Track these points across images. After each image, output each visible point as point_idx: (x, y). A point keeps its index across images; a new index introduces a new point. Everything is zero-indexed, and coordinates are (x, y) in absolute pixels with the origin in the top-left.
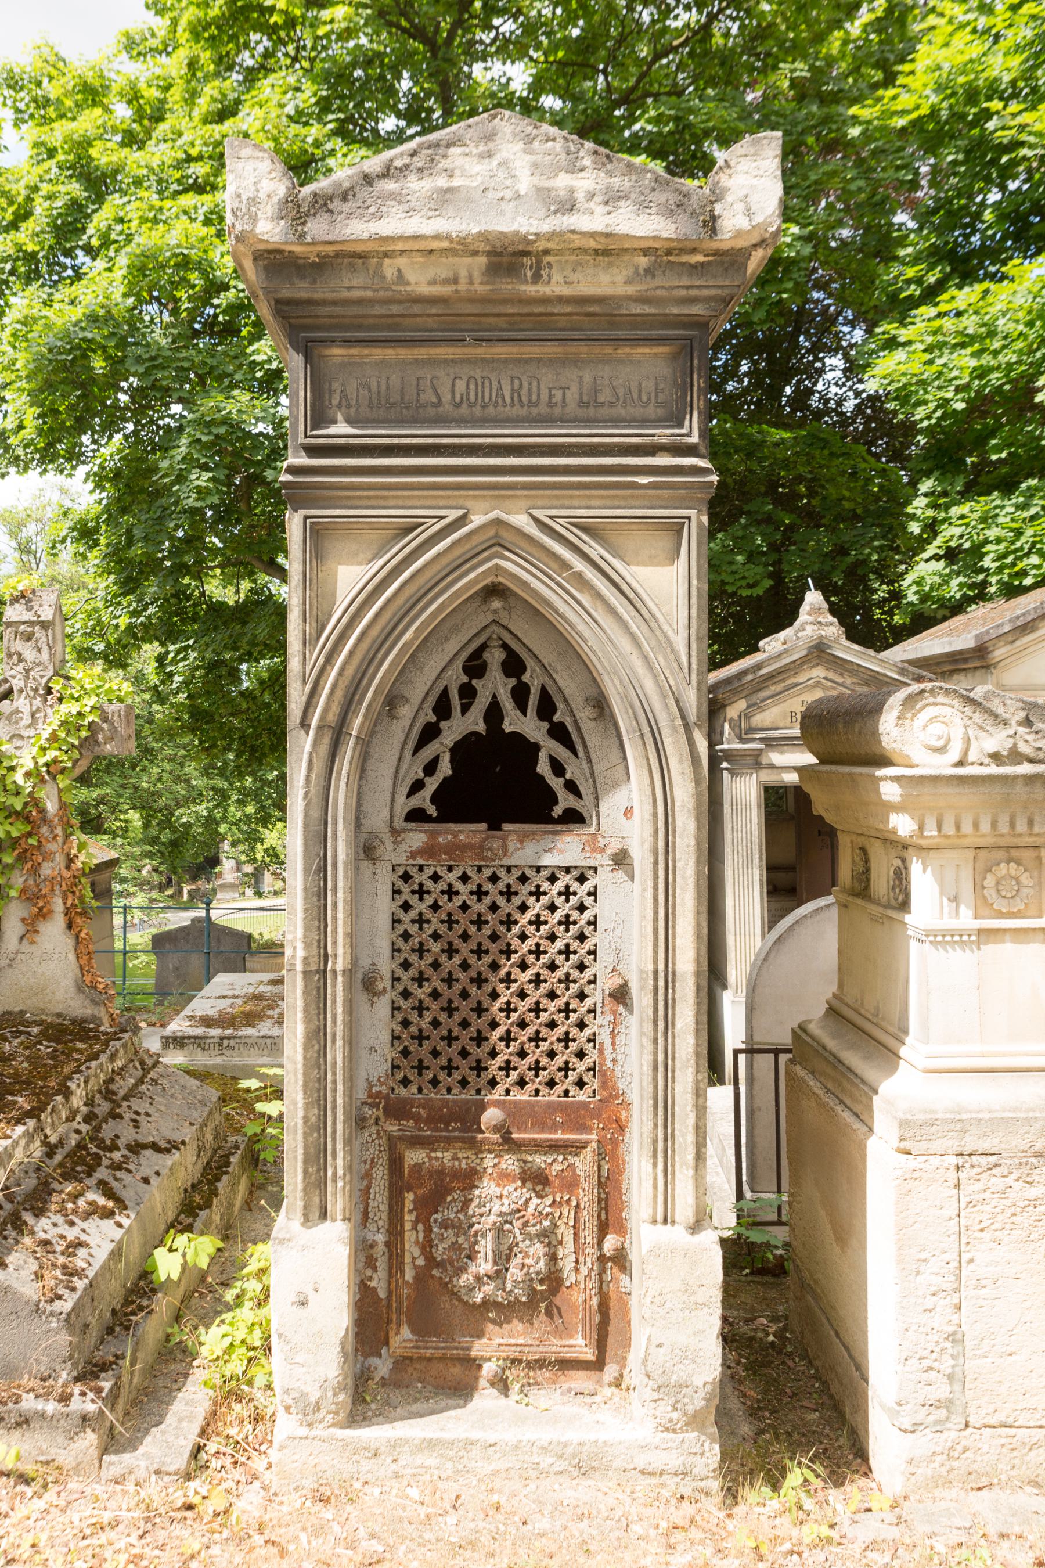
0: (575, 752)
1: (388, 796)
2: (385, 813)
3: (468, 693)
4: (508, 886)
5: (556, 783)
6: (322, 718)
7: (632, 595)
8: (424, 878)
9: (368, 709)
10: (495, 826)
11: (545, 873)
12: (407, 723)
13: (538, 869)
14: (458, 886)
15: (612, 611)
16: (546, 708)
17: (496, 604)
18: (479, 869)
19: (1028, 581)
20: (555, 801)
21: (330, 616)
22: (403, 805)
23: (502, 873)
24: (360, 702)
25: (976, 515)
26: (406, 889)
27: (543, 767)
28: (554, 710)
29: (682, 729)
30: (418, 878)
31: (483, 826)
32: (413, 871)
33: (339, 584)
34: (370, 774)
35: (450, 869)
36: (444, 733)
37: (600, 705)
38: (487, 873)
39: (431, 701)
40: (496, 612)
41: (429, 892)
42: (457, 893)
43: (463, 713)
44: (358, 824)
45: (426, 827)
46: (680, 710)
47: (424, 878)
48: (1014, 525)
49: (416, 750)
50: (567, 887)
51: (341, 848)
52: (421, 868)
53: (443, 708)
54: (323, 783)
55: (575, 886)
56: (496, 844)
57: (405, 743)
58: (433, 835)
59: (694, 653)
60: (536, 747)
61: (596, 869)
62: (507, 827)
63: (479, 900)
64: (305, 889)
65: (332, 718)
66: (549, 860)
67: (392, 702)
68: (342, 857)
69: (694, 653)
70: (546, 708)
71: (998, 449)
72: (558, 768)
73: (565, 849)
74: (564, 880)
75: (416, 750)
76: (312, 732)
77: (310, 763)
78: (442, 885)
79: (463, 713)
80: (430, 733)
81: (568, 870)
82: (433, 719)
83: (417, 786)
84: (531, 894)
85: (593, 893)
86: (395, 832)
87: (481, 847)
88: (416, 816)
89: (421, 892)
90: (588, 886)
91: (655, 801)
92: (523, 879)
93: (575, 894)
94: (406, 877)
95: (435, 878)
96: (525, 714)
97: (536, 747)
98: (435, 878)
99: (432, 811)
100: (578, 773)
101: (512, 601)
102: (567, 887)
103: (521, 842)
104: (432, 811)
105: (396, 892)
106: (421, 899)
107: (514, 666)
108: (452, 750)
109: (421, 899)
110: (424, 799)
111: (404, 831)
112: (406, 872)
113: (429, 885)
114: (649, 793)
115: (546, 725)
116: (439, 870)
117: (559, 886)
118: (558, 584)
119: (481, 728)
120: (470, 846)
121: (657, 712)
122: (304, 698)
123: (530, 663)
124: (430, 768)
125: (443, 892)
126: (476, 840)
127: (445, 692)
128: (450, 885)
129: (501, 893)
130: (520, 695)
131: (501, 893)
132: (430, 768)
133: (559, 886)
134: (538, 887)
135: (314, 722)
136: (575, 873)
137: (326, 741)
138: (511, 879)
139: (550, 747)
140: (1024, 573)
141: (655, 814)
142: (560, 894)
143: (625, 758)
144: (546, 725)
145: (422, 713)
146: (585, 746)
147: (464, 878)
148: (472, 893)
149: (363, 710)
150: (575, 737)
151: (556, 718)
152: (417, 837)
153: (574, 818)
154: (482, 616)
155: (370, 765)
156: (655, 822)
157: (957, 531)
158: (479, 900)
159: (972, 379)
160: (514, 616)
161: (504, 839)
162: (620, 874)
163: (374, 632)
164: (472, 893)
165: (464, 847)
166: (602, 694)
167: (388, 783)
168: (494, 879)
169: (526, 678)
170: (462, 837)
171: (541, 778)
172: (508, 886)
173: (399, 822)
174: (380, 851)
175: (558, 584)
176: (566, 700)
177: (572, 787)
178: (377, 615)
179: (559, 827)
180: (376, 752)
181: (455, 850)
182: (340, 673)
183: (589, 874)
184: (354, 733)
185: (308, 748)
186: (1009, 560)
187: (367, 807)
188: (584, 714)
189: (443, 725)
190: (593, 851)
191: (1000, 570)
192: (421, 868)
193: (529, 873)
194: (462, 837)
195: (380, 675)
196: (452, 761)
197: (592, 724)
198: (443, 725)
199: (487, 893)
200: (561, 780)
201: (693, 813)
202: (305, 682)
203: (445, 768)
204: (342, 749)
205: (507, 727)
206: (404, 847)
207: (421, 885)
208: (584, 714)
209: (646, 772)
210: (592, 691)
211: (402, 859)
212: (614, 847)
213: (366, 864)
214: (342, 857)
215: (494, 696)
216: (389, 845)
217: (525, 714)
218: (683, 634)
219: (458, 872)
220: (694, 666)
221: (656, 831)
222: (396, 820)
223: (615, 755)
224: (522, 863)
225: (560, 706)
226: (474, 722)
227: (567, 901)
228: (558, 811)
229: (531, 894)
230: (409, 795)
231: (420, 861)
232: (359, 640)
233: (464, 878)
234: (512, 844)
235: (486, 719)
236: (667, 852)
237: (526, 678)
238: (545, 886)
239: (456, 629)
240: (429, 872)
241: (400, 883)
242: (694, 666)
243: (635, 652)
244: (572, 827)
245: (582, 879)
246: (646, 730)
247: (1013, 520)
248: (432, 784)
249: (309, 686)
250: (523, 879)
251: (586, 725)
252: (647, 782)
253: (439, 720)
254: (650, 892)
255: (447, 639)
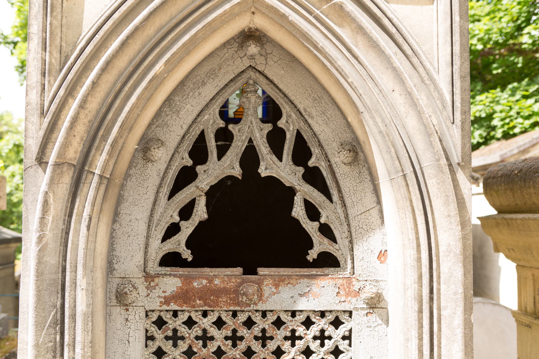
0: (329, 197)
1: (142, 240)
2: (139, 258)
3: (224, 137)
4: (264, 331)
5: (311, 228)
6: (60, 155)
7: (393, 30)
8: (178, 323)
9: (113, 146)
10: (250, 270)
11: (301, 318)
12: (163, 167)
13: (294, 314)
14: (213, 331)
15: (374, 45)
16: (301, 154)
17: (253, 49)
18: (235, 314)
19: (517, 130)
20: (311, 246)
21: (75, 47)
22: (158, 249)
23: (257, 318)
24: (105, 138)
25: (489, 100)
26: (159, 335)
27: (298, 211)
28: (309, 155)
29: (446, 169)
30: (172, 323)
31: (239, 270)
32: (167, 317)
33: (86, 15)
34: (124, 218)
35: (205, 314)
36: (200, 177)
37: (356, 150)
38: (242, 318)
39: (188, 144)
40: (252, 57)
41: (183, 338)
42: (212, 338)
43: (220, 158)
44: (110, 268)
45: (181, 271)
46: (444, 151)
47: (178, 323)
48: (509, 104)
49: (172, 195)
50: (322, 331)
51: (82, 298)
52: (175, 314)
53: (199, 153)
54: (61, 226)
55: (330, 330)
56: (252, 289)
57: (160, 186)
58: (187, 279)
59: (457, 91)
60: (291, 192)
61: (350, 313)
62: (262, 271)
63: (234, 345)
64: (37, 346)
65: (74, 153)
66: (305, 305)
67: (146, 146)
68: (81, 307)
69: (457, 91)
70: (301, 154)
71: (497, 68)
72: (313, 213)
73: (320, 293)
74: (320, 324)
75: (172, 195)
76: (49, 169)
77: (46, 203)
78: (197, 331)
79: (220, 158)
80: (186, 177)
81: (323, 314)
82: (189, 163)
83: (173, 230)
84: (286, 338)
85: (347, 337)
86: (148, 277)
87: (236, 292)
88: (171, 260)
89: (175, 338)
90: (342, 330)
91: (418, 246)
92: (279, 323)
93: (330, 338)
94: (160, 323)
95: (190, 323)
96: (281, 159)
97: (291, 192)
98: (190, 323)
99: (187, 255)
100: (333, 217)
101: (269, 48)
102: (322, 331)
103: (277, 286)
104: (187, 255)
105: (150, 338)
106: (175, 345)
107: (272, 112)
108: (207, 194)
109: (175, 345)
110: (179, 243)
111: (158, 275)
112: (160, 318)
113: (183, 330)
114: (412, 237)
115: (301, 170)
116: (194, 316)
117: (314, 330)
118: (317, 18)
119: (237, 172)
120: (225, 291)
121: (420, 153)
122: (42, 133)
123: (286, 109)
124: (186, 212)
125: (197, 338)
126: (231, 285)
127: (202, 137)
128: (205, 331)
129: (256, 338)
130: (276, 140)
131: (256, 338)
132: (186, 212)
133: (314, 330)
134: (293, 331)
135: (52, 157)
136: (331, 317)
137: (67, 179)
138: (266, 324)
139: (305, 191)
140: (514, 127)
141: (419, 259)
142: (315, 338)
143: (379, 202)
144: (301, 170)
145: (178, 158)
146: (340, 191)
147: (219, 323)
148: (227, 338)
149: (107, 147)
150: (329, 182)
151: (311, 163)
152: (171, 282)
153: (328, 261)
154: (238, 62)
155: (124, 209)
156: (420, 267)
157: (480, 107)
158: (234, 345)
159: (485, 35)
160: (271, 62)
161: (260, 284)
162: (374, 318)
163: (122, 63)
164: (227, 338)
165: (219, 292)
166: (356, 139)
167: (142, 227)
168: (249, 323)
169: (281, 123)
170: (217, 282)
171: (297, 222)
172: (264, 331)
173: (154, 267)
174: (131, 298)
175: (317, 18)
176: (321, 145)
177: (326, 231)
178: (124, 44)
179: (314, 271)
180: (130, 194)
181: (210, 295)
182: (82, 106)
183: (343, 318)
184: (97, 171)
185: (44, 187)
186: (507, 121)
187: (120, 251)
188: (339, 159)
189: (199, 169)
190: (348, 294)
191: (503, 126)
192: (175, 314)
193: (284, 317)
194: (217, 282)
195: (127, 109)
196: (207, 205)
197: (347, 169)
198: (199, 169)
199: (242, 338)
200: (316, 224)
201: (461, 258)
202: (43, 114)
203: (201, 212)
204: (84, 188)
205: (263, 172)
206: (158, 292)
207: (175, 331)
208: (339, 159)
209: (410, 215)
210: (347, 137)
211: (155, 304)
212: (369, 292)
213: (118, 311)
214: (81, 307)
215: (250, 141)
216: (142, 290)
217: (281, 159)
218: (445, 71)
219: (212, 317)
220: (458, 104)
221: (420, 277)
222: (150, 264)
223: (369, 200)
224: (277, 307)
225: (315, 150)
226: (230, 166)
227: (322, 345)
228: (312, 255)
229: (286, 338)
230: (164, 239)
231: (174, 307)
232: (104, 70)
233: (219, 323)
234: (268, 289)
235: (242, 164)
236: (431, 299)
237: (281, 123)
238: (301, 330)
239: (213, 74)
240: (184, 317)
241: (154, 329)
242: (458, 104)
243: (398, 88)
244: (327, 270)
245: (337, 323)
246: (409, 170)
247: (508, 102)
248: (188, 228)
249: (47, 120)
250: (279, 323)
251: (341, 170)
252: (411, 225)
253: (196, 164)
254: (414, 342)
255: (204, 84)
